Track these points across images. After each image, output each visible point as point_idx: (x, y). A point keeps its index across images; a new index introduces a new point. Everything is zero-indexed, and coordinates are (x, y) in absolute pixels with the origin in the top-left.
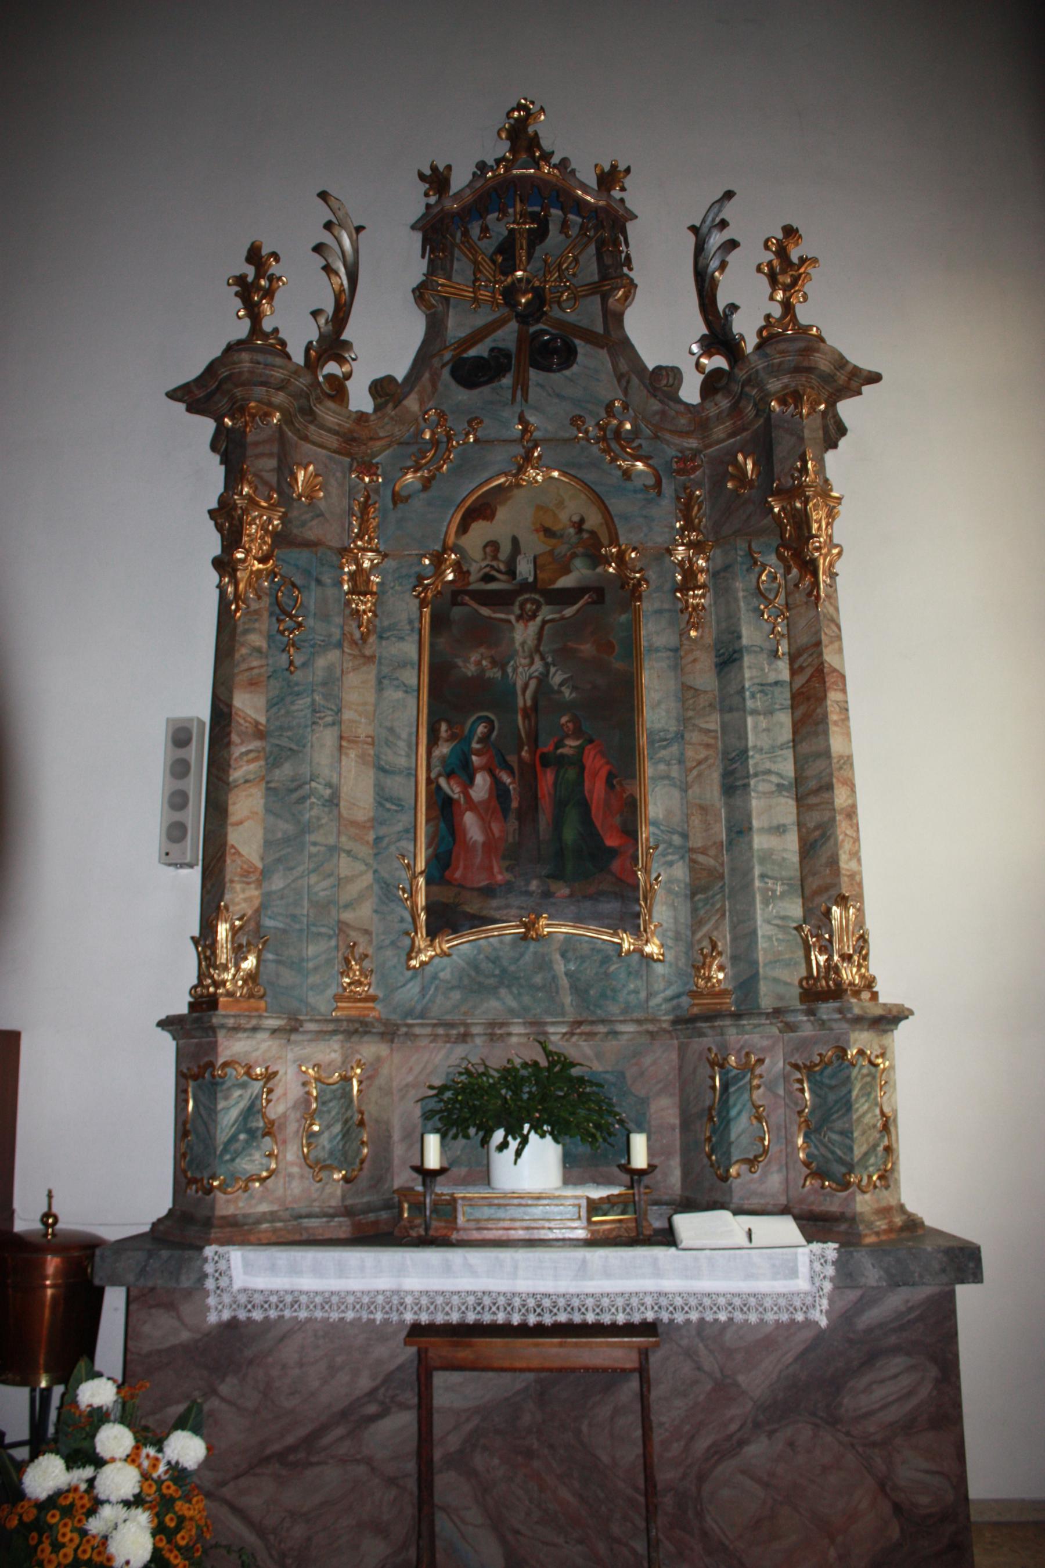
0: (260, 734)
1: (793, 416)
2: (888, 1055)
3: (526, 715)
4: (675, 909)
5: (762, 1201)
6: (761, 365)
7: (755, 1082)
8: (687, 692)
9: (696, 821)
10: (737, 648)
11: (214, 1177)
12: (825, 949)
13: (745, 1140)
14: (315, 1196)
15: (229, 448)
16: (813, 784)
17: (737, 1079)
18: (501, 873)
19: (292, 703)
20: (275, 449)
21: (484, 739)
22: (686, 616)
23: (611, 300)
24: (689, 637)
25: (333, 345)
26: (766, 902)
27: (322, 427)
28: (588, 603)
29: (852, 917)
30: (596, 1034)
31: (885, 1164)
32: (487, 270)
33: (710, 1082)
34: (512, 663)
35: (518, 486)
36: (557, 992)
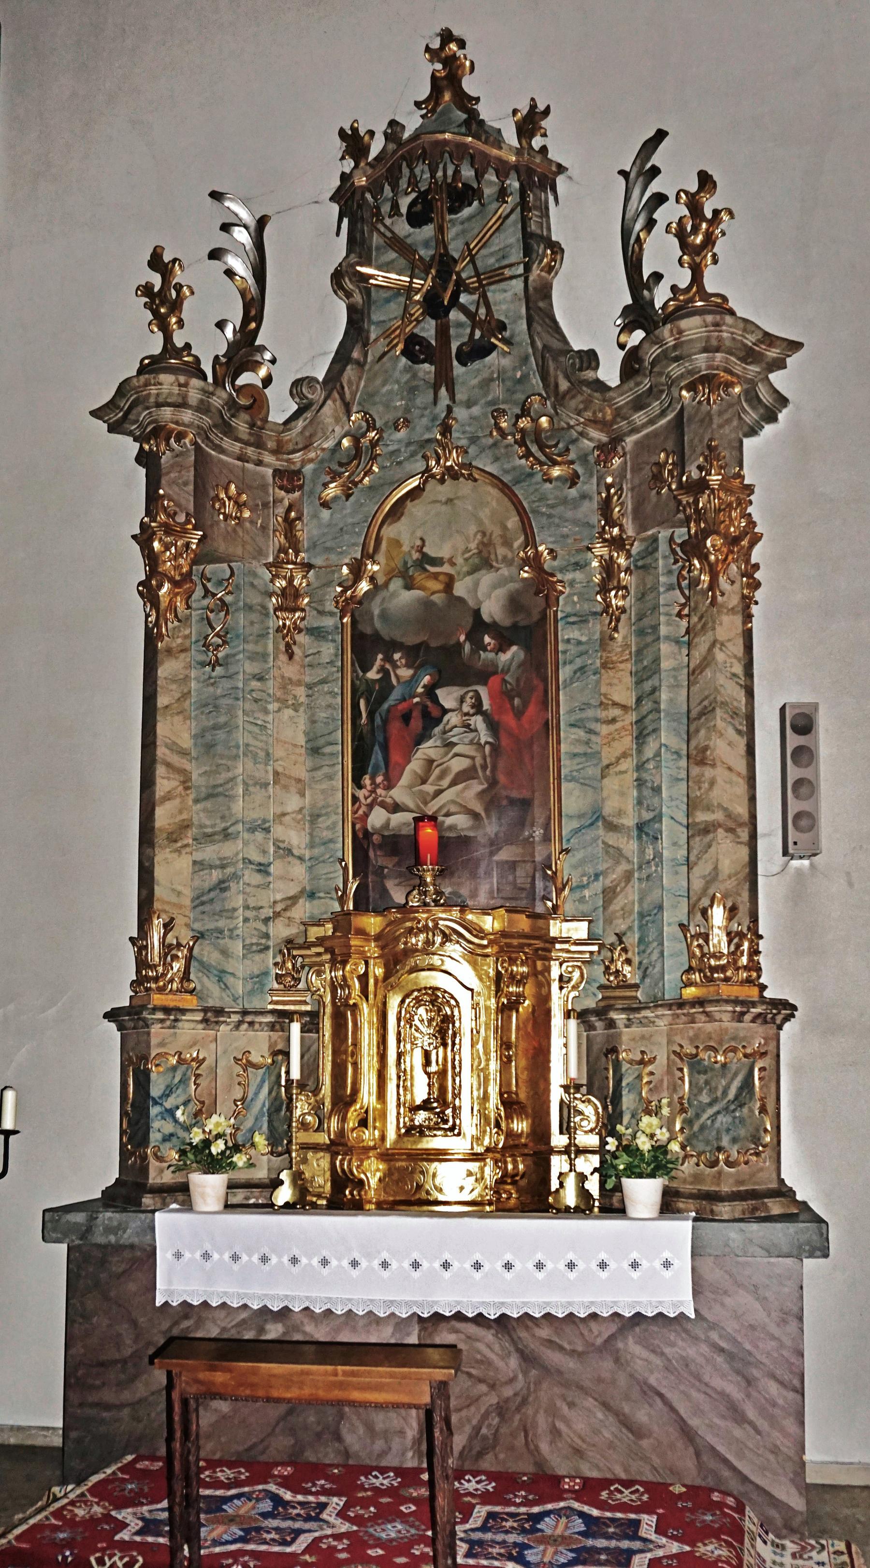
25: (243, 352)
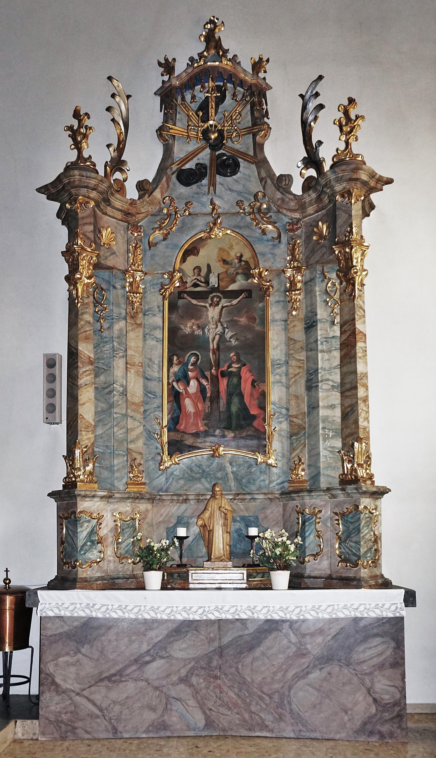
0: (91, 363)
1: (347, 204)
2: (378, 509)
3: (214, 353)
4: (282, 443)
5: (319, 573)
6: (332, 177)
7: (318, 520)
8: (290, 341)
9: (293, 403)
10: (315, 320)
11: (77, 561)
12: (350, 461)
13: (312, 546)
14: (120, 570)
15: (68, 218)
16: (348, 386)
17: (309, 519)
18: (202, 426)
19: (104, 346)
20: (92, 220)
21: (194, 364)
22: (291, 304)
23: (258, 137)
24: (292, 315)
25: (117, 164)
26: (325, 440)
27: (114, 208)
28: (244, 298)
29: (364, 448)
30: (245, 499)
31: (375, 557)
32: (195, 119)
33: (297, 521)
34: (207, 327)
35: (210, 238)
36: (228, 481)
